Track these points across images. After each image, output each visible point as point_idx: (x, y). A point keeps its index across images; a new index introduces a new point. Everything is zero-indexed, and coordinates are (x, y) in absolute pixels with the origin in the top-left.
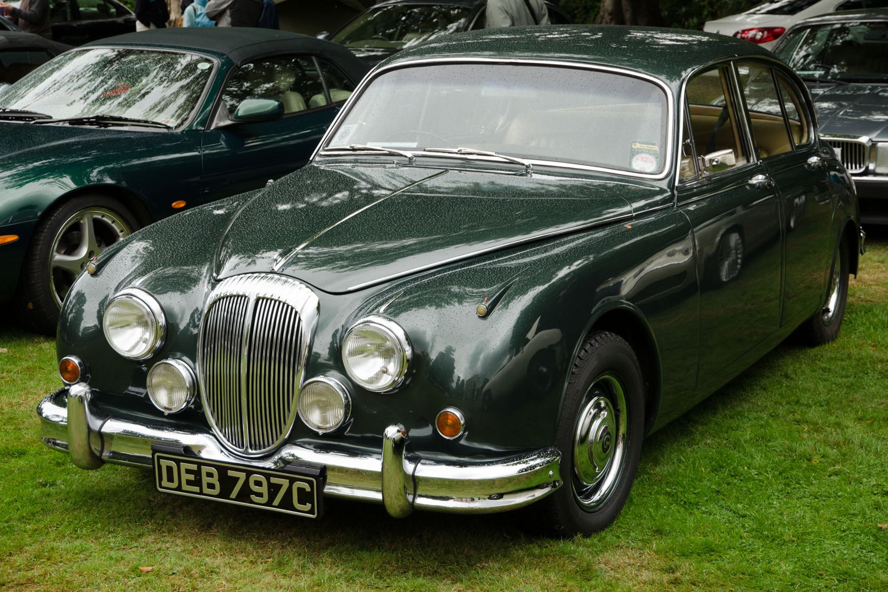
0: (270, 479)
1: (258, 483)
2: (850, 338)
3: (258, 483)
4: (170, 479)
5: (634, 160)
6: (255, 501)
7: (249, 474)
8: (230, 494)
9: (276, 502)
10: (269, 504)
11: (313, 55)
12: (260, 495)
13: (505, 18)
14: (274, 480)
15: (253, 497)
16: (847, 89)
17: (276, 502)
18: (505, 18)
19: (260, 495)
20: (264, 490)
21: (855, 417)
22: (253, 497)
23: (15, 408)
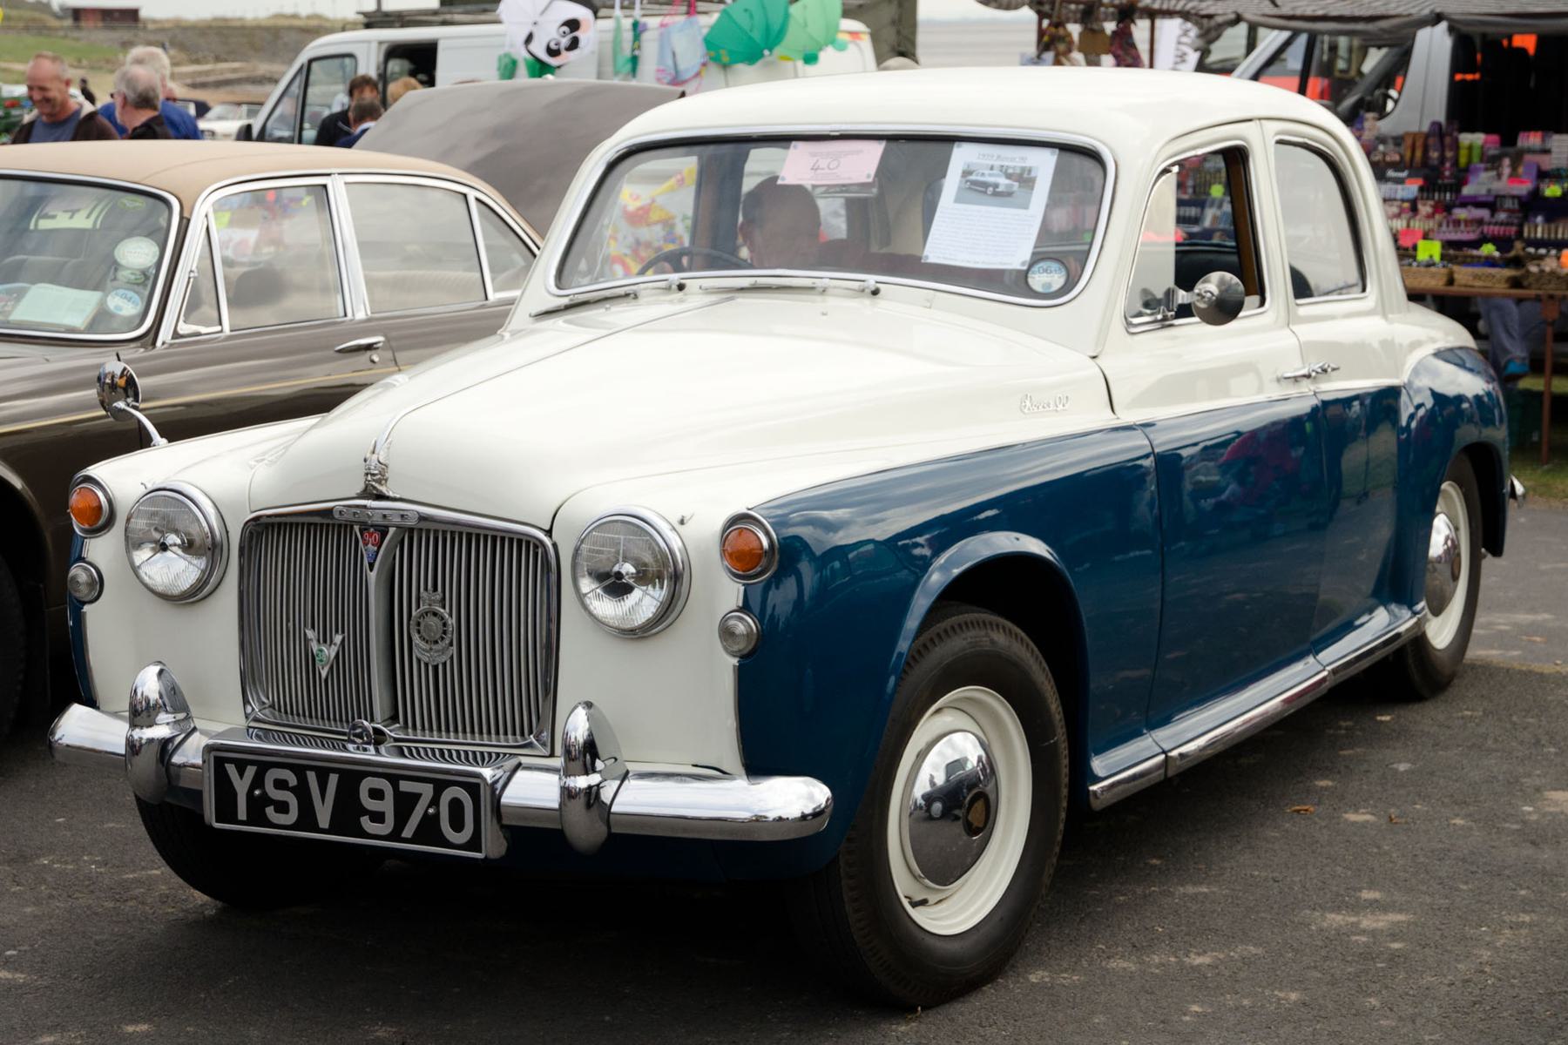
0: (398, 785)
1: (377, 794)
2: (1098, 1023)
3: (377, 794)
4: (457, 825)
5: (1030, 281)
6: (275, 822)
7: (263, 768)
8: (403, 829)
9: (408, 832)
10: (395, 835)
11: (1082, 774)
12: (378, 817)
13: (343, 105)
14: (405, 786)
15: (365, 821)
16: (1378, 921)
17: (408, 832)
18: (343, 105)
19: (378, 817)
20: (387, 806)
21: (1333, 927)
22: (365, 821)
23: (1488, 939)
